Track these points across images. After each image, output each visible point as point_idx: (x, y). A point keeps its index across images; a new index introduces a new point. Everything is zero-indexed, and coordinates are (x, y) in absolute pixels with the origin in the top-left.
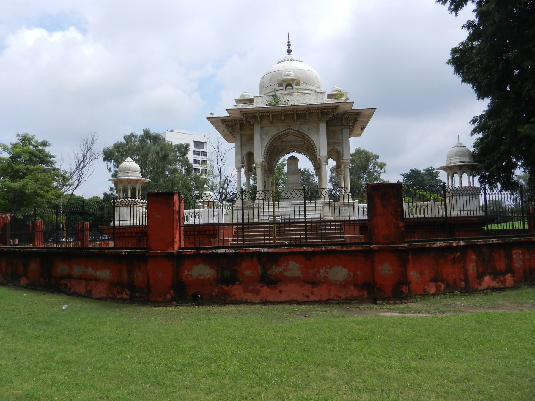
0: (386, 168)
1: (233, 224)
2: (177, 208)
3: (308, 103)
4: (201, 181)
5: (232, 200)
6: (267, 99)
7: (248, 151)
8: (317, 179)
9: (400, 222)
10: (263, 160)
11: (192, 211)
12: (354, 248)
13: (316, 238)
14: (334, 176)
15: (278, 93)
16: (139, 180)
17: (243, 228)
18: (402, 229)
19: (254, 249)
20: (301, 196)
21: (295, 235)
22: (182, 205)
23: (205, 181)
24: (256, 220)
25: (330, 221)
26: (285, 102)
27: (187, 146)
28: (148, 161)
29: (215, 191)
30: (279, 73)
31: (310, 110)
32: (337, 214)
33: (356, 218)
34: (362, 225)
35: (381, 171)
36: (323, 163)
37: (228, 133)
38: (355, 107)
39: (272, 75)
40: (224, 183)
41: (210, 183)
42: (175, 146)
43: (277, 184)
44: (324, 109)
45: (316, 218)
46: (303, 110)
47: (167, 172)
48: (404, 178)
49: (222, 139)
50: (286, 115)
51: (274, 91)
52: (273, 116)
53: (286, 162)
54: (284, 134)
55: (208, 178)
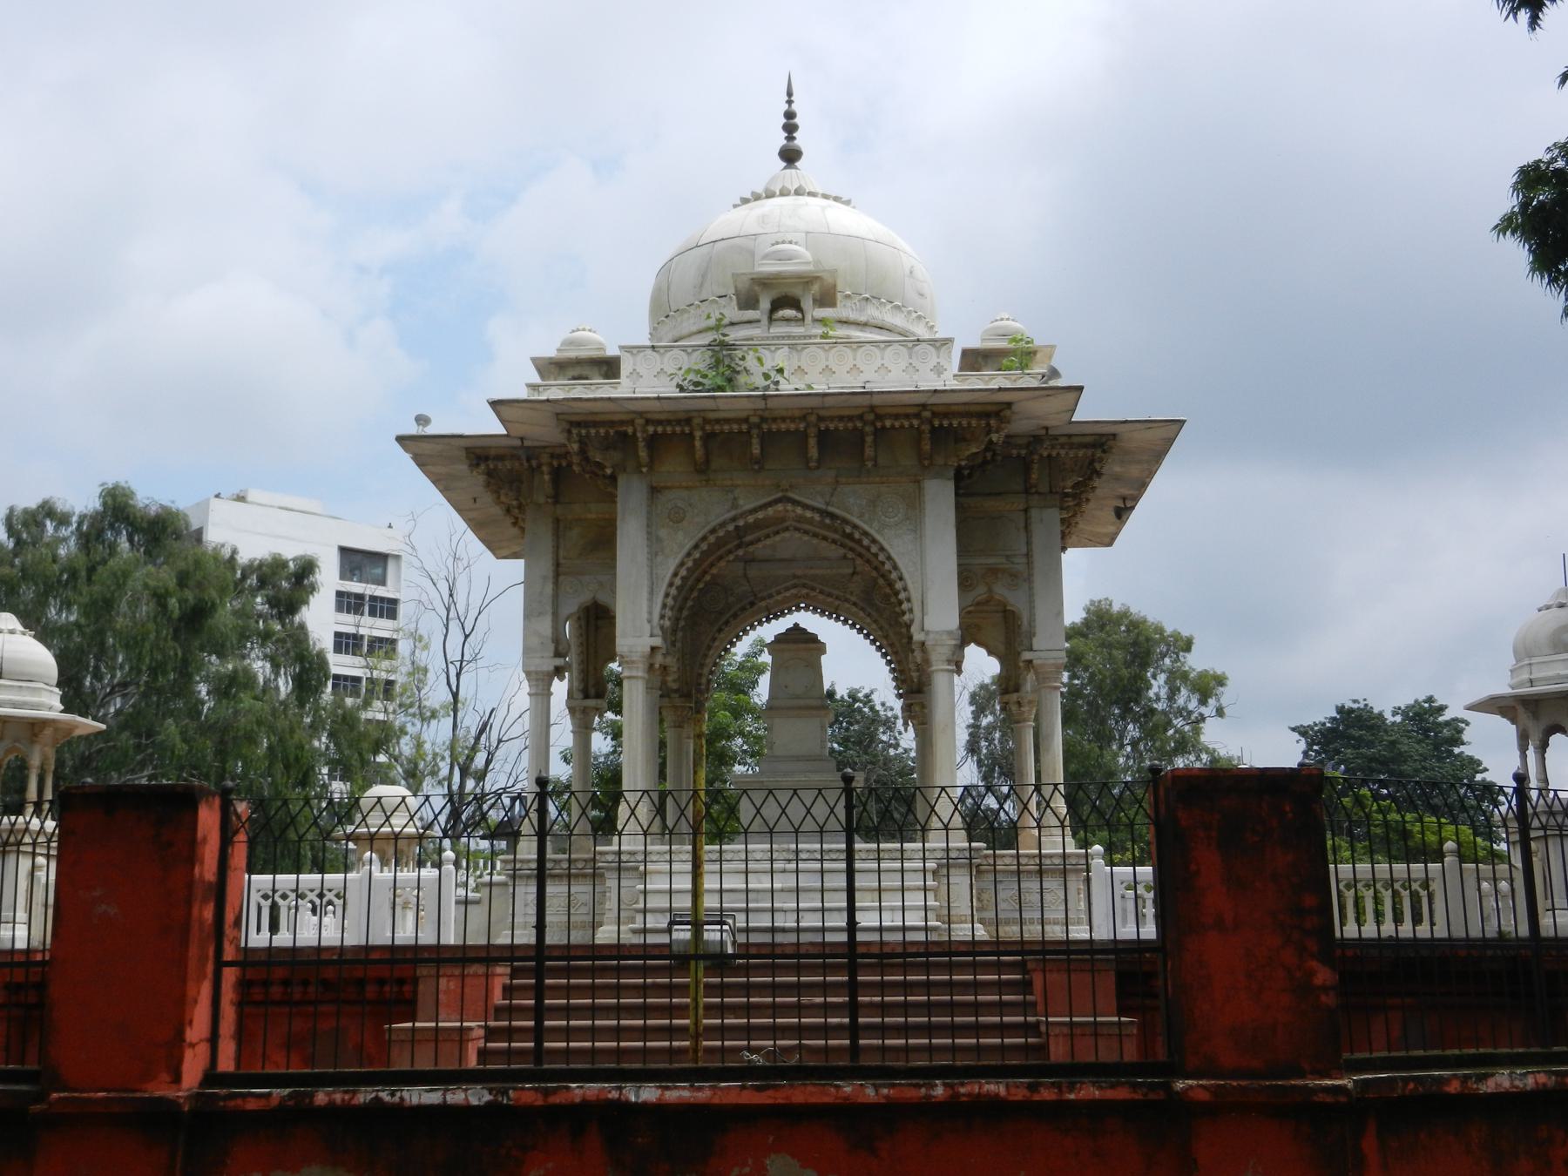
0: (1227, 696)
1: (489, 955)
2: (208, 868)
4: (363, 736)
5: (507, 831)
6: (686, 361)
8: (908, 739)
9: (1314, 964)
10: (658, 641)
11: (310, 879)
12: (1089, 1091)
13: (905, 1030)
14: (991, 729)
15: (734, 335)
16: (44, 723)
17: (539, 973)
18: (1329, 1000)
19: (593, 1089)
20: (833, 824)
21: (799, 1010)
22: (239, 854)
23: (385, 736)
24: (606, 934)
25: (973, 947)
26: (766, 376)
27: (306, 568)
28: (116, 633)
29: (428, 786)
30: (742, 245)
31: (879, 417)
32: (1007, 908)
33: (1102, 933)
34: (1124, 965)
35: (1205, 711)
36: (938, 664)
37: (497, 511)
38: (1085, 412)
39: (709, 257)
40: (474, 749)
41: (405, 747)
42: (248, 570)
43: (723, 759)
44: (946, 415)
45: (904, 929)
46: (851, 418)
47: (203, 689)
48: (1310, 746)
49: (473, 545)
50: (768, 439)
51: (716, 328)
52: (708, 438)
53: (766, 658)
54: (757, 526)
55: (399, 720)
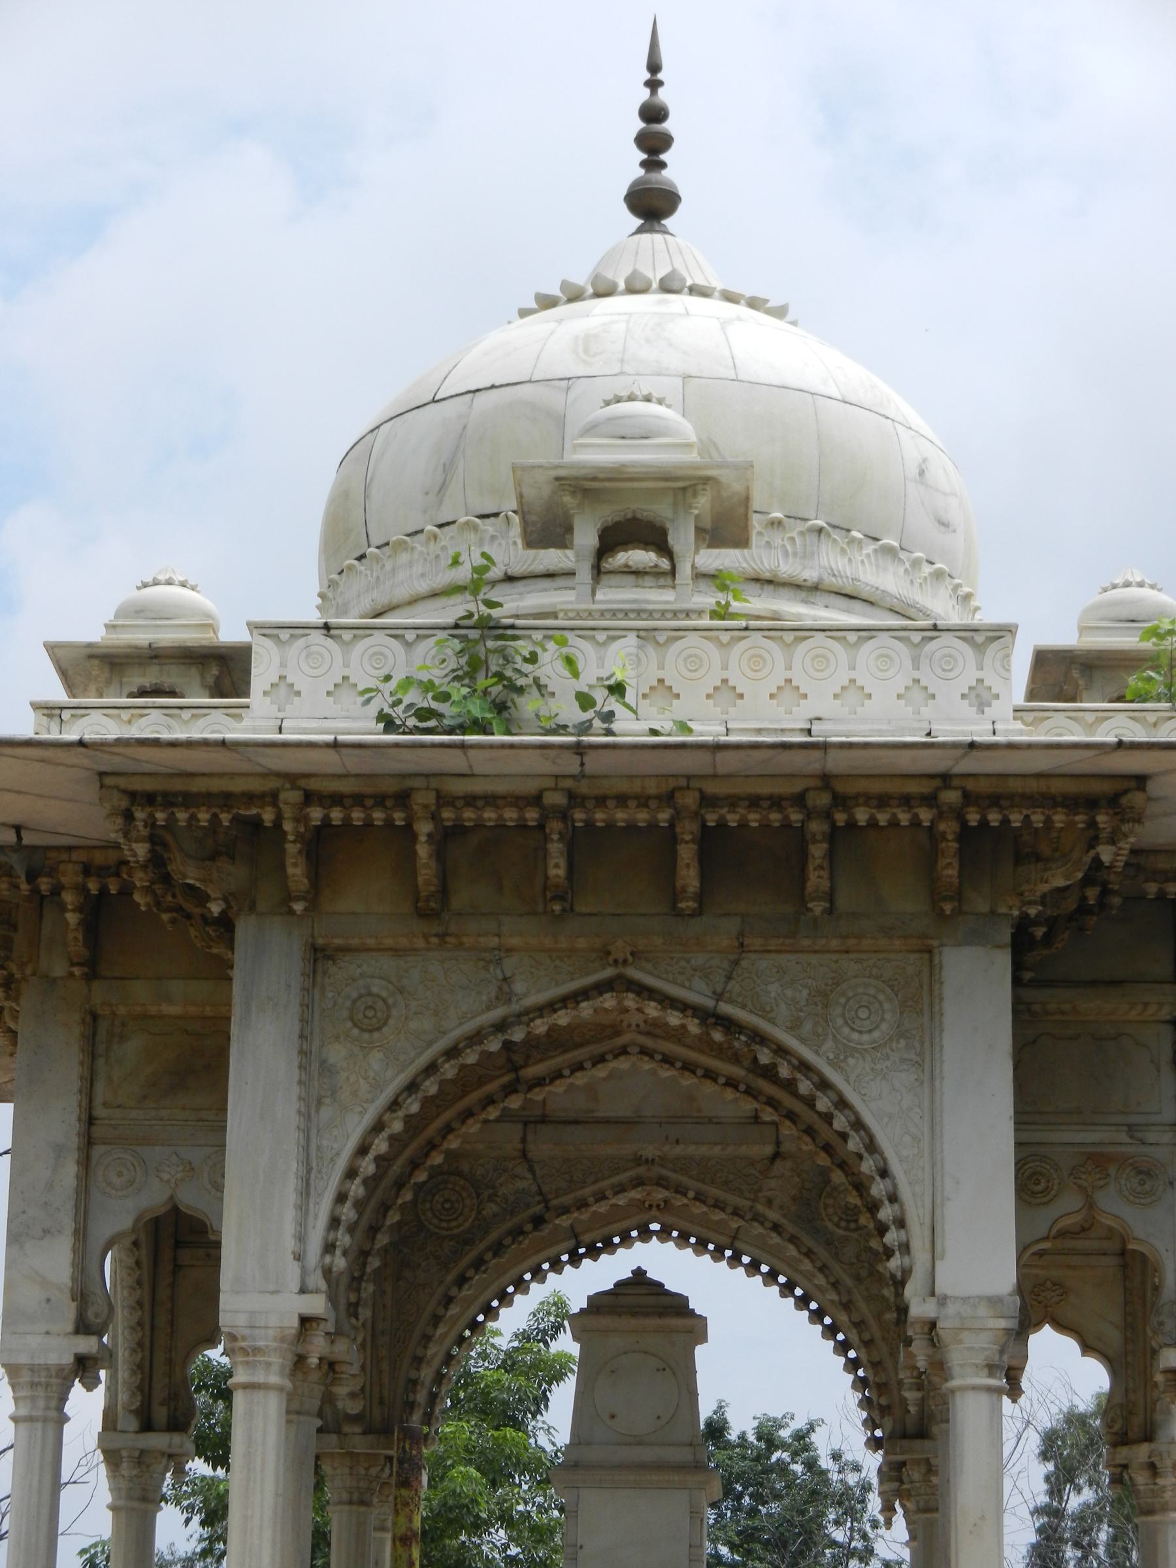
3: (824, 732)
6: (402, 662)
7: (153, 1197)
10: (317, 1305)
14: (1086, 1521)
26: (585, 701)
30: (535, 402)
31: (841, 801)
39: (457, 421)
44: (995, 800)
46: (776, 802)
50: (586, 844)
51: (473, 587)
52: (448, 837)
53: (566, 1344)
54: (556, 1041)
